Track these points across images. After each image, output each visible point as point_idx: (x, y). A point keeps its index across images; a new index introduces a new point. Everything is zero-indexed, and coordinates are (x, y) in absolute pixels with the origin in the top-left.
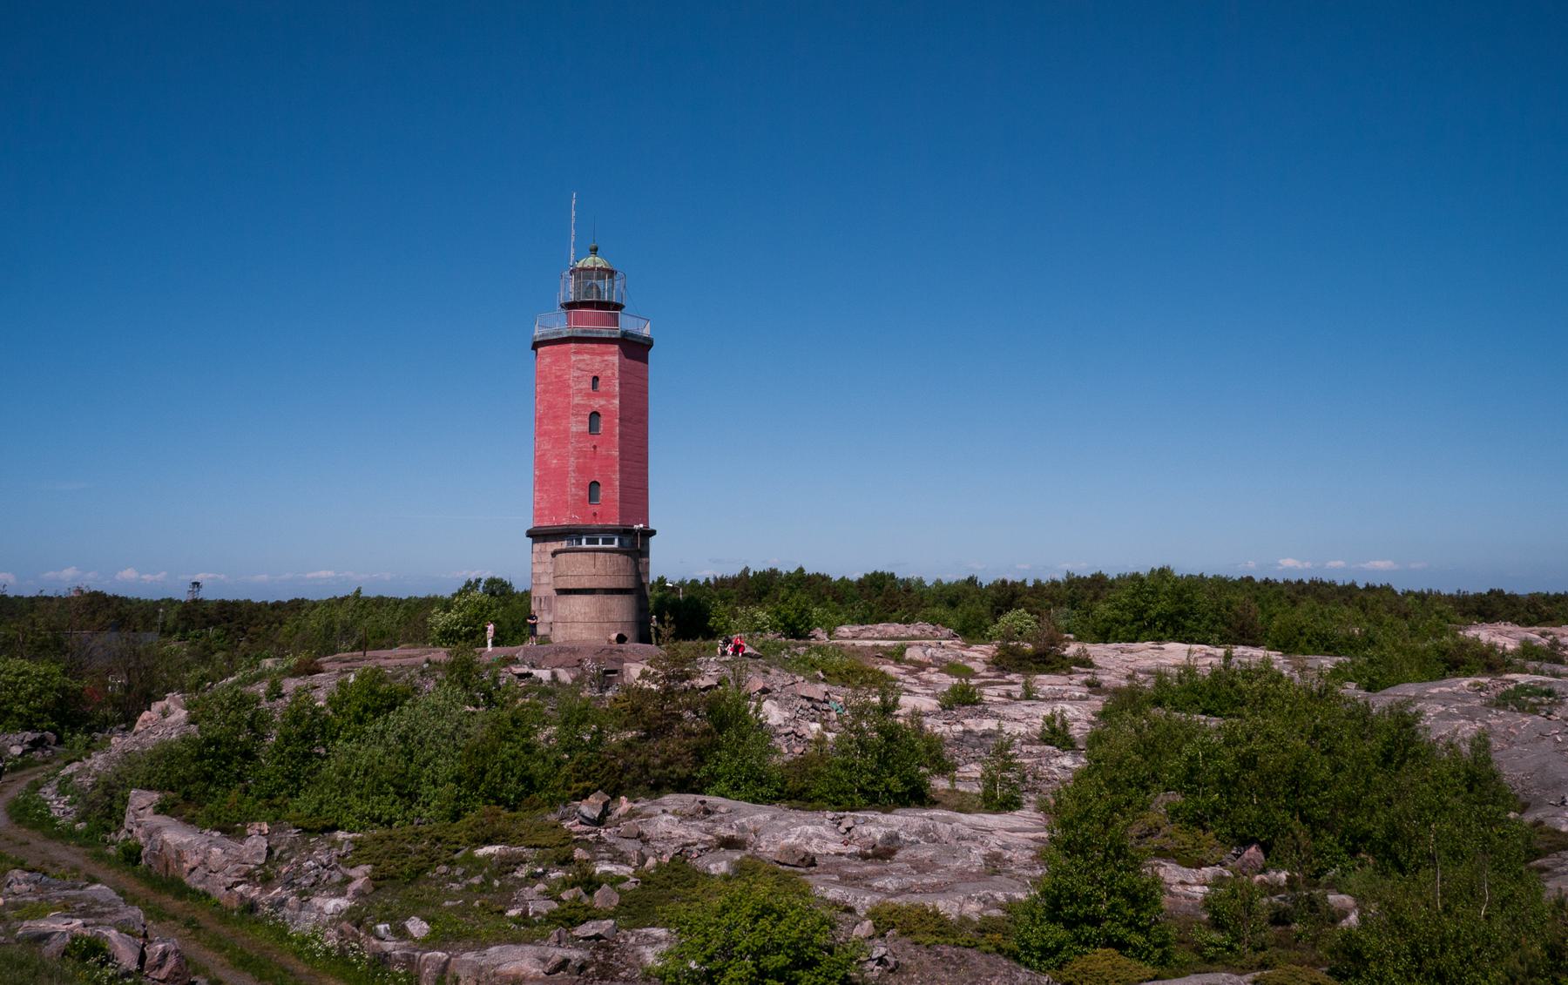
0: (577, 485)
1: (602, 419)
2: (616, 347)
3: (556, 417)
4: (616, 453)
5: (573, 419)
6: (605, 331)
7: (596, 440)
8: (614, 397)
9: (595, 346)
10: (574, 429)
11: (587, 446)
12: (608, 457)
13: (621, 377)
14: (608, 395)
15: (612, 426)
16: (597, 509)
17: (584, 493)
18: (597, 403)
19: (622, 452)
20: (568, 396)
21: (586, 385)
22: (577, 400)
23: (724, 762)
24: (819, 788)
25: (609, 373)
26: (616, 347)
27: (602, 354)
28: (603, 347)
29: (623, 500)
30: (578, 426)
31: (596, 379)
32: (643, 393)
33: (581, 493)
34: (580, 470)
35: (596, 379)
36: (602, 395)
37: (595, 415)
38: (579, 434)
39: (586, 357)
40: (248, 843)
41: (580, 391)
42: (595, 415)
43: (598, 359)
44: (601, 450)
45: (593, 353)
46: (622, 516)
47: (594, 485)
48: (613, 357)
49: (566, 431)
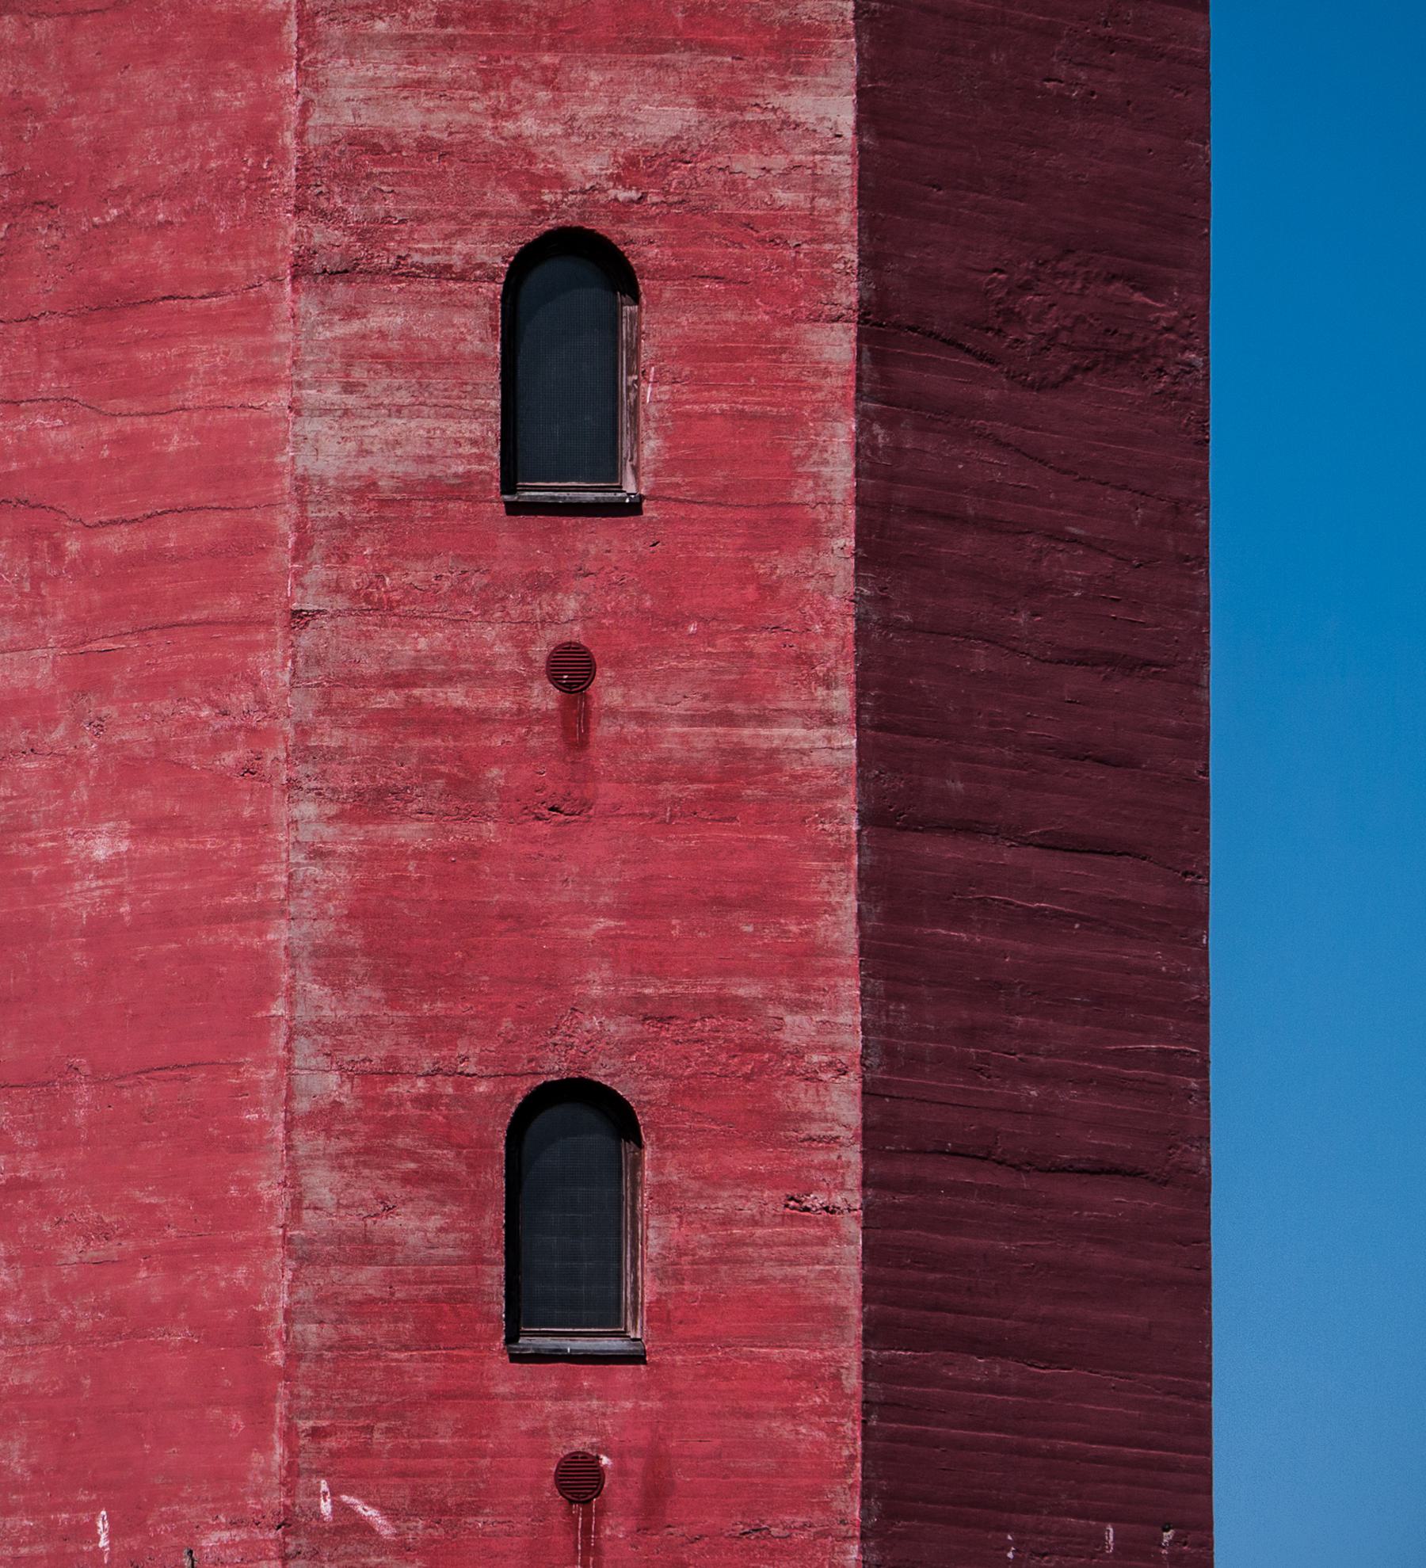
0: (371, 1133)
1: (659, 326)
3: (111, 304)
4: (820, 741)
5: (307, 323)
7: (587, 580)
10: (322, 449)
11: (485, 651)
12: (734, 786)
15: (770, 403)
16: (599, 1415)
17: (441, 1232)
19: (890, 716)
24: (422, 509)
29: (905, 1303)
30: (370, 405)
33: (417, 1226)
34: (403, 943)
37: (567, 285)
38: (390, 511)
40: (383, 1053)
42: (567, 285)
44: (655, 709)
47: (564, 1152)
49: (235, 467)
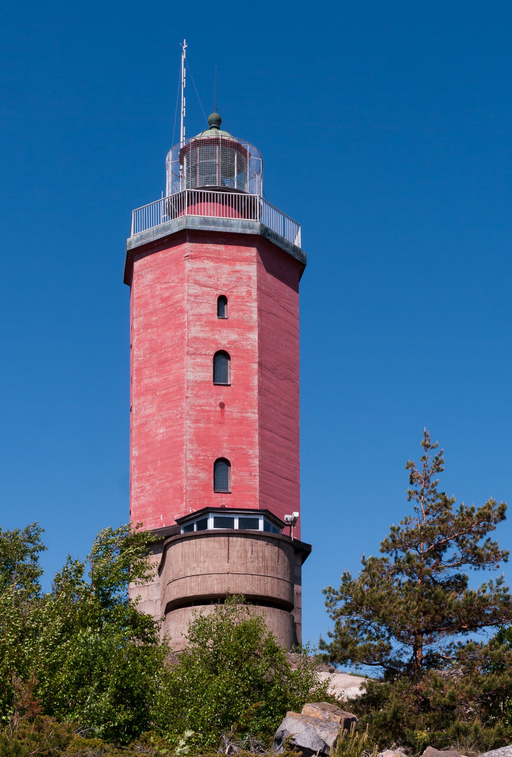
0: (196, 463)
1: (232, 363)
2: (253, 252)
3: (163, 362)
4: (253, 416)
5: (189, 361)
6: (237, 224)
8: (250, 329)
9: (221, 248)
10: (190, 376)
11: (211, 400)
12: (242, 421)
13: (260, 300)
14: (243, 326)
15: (245, 372)
17: (206, 476)
18: (225, 338)
20: (181, 325)
21: (210, 307)
22: (195, 331)
23: (505, 557)
25: (242, 291)
26: (253, 252)
27: (233, 260)
28: (233, 250)
30: (197, 370)
31: (222, 300)
32: (293, 438)
34: (200, 439)
35: (222, 300)
36: (231, 326)
37: (221, 356)
38: (199, 385)
39: (208, 264)
41: (199, 317)
42: (221, 356)
43: (226, 268)
44: (232, 411)
45: (218, 259)
46: (264, 489)
47: (222, 463)
48: (245, 269)
49: (179, 380)
